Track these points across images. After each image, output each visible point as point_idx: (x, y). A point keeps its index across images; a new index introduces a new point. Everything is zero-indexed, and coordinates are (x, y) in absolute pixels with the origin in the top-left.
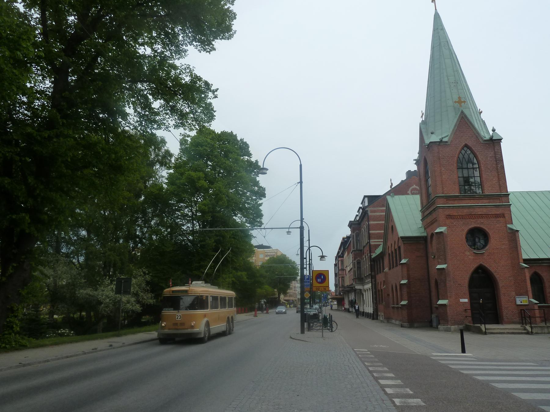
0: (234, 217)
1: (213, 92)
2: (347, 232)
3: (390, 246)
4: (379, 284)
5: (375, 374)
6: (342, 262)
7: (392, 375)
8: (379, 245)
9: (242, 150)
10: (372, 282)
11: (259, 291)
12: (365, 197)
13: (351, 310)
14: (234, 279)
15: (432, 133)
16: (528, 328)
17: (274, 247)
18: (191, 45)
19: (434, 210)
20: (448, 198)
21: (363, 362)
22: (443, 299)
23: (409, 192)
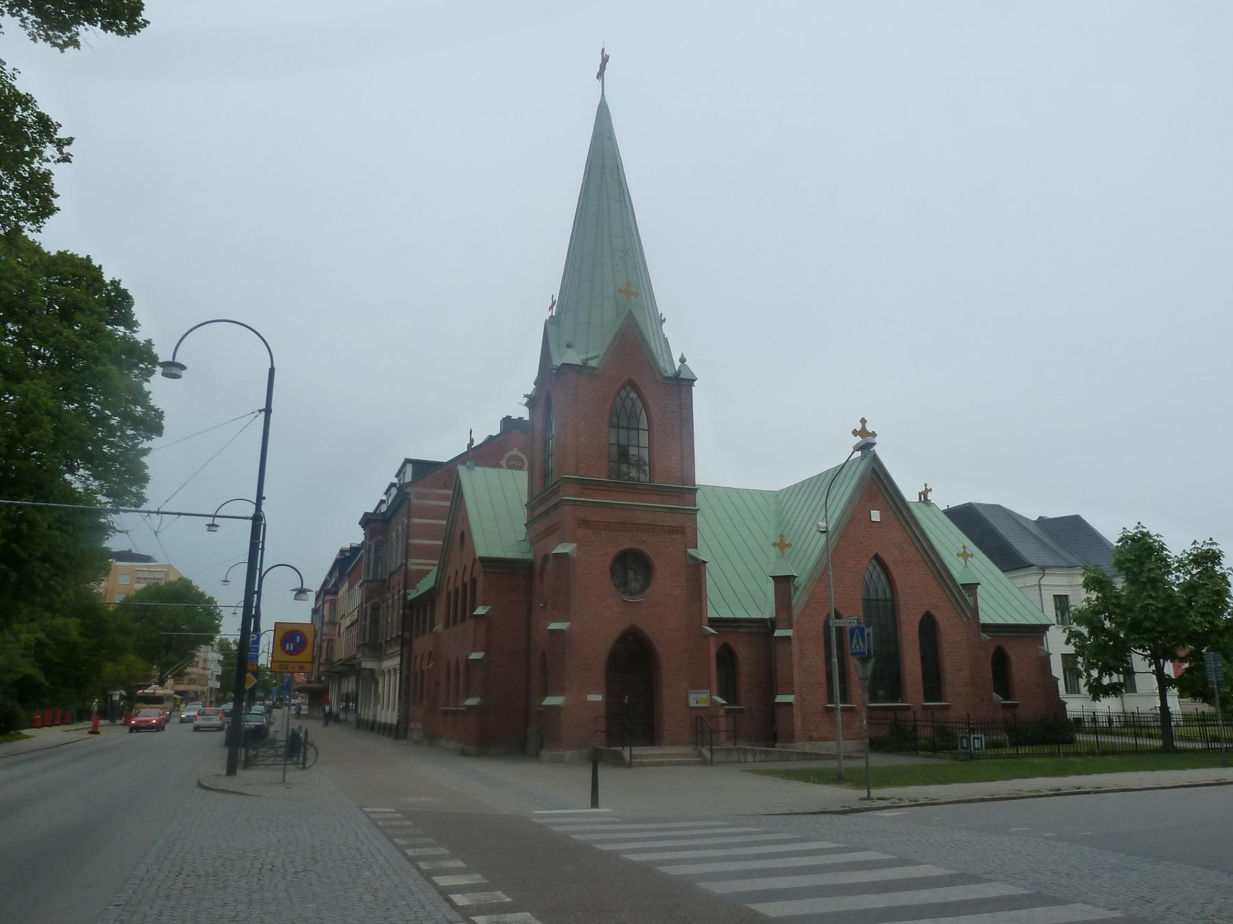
0: (68, 477)
1: (60, 144)
2: (357, 536)
3: (453, 576)
4: (419, 658)
5: (422, 865)
6: (334, 605)
7: (460, 864)
8: (427, 572)
9: (112, 308)
10: (401, 655)
11: (109, 667)
12: (407, 461)
13: (342, 716)
14: (42, 636)
15: (568, 346)
16: (706, 752)
17: (161, 560)
18: (13, 15)
19: (555, 506)
20: (587, 485)
21: (390, 838)
22: (556, 693)
23: (503, 462)
